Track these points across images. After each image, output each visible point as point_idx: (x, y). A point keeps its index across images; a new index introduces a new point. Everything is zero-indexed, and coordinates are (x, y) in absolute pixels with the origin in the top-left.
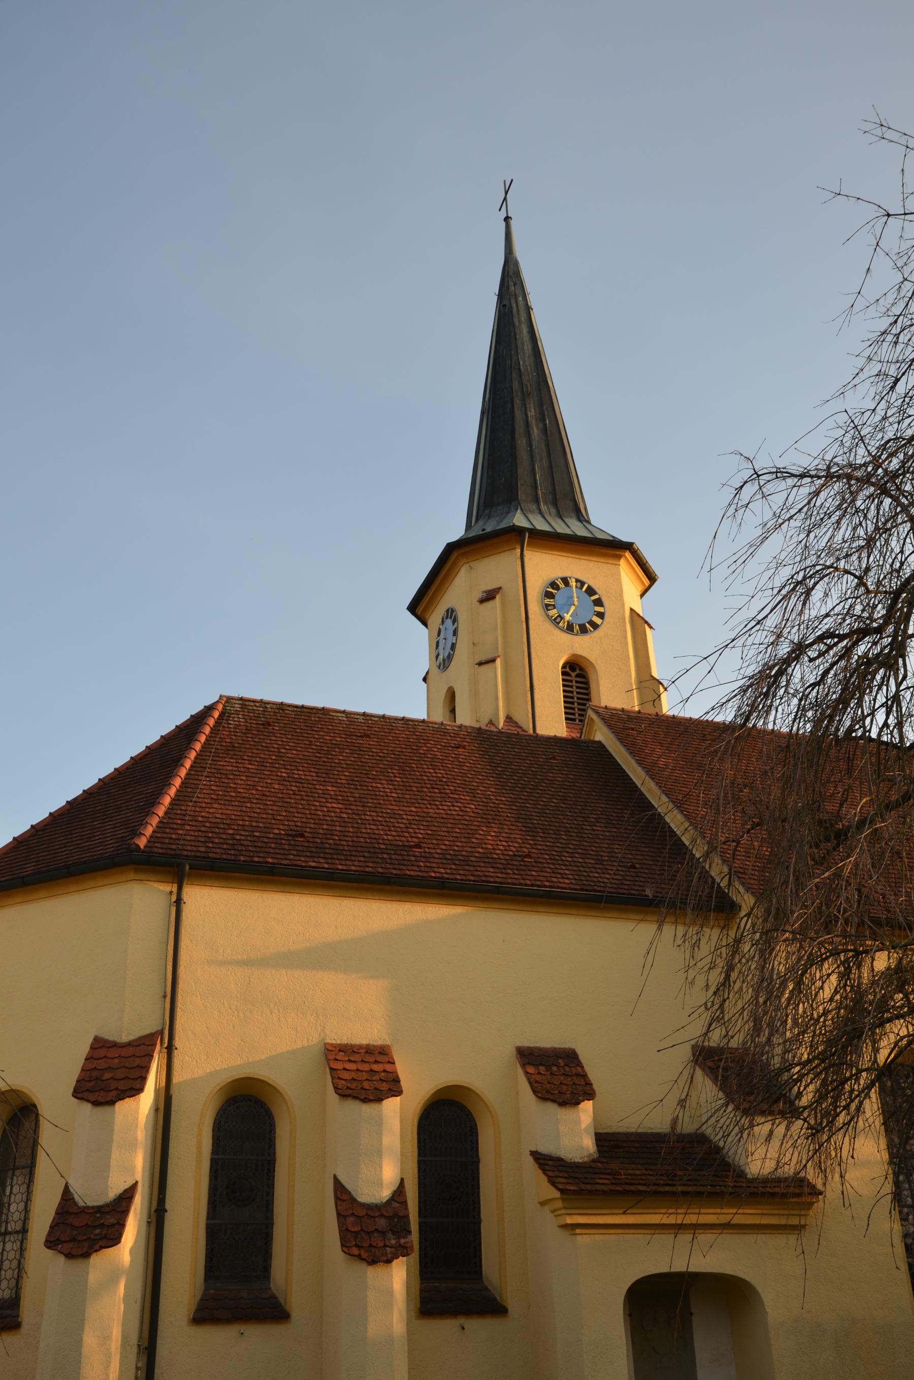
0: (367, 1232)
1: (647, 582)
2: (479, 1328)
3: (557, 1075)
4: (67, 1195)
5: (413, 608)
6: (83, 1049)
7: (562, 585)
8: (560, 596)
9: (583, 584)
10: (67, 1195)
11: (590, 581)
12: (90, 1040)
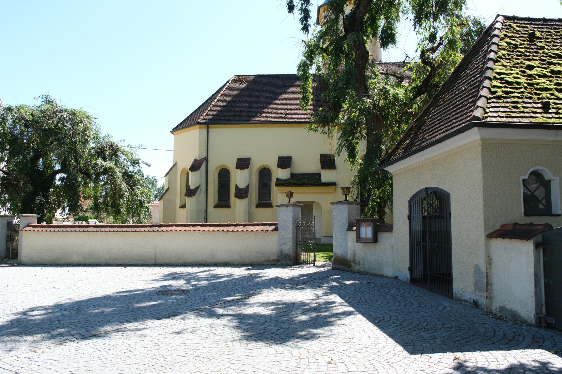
2: (268, 210)
4: (237, 187)
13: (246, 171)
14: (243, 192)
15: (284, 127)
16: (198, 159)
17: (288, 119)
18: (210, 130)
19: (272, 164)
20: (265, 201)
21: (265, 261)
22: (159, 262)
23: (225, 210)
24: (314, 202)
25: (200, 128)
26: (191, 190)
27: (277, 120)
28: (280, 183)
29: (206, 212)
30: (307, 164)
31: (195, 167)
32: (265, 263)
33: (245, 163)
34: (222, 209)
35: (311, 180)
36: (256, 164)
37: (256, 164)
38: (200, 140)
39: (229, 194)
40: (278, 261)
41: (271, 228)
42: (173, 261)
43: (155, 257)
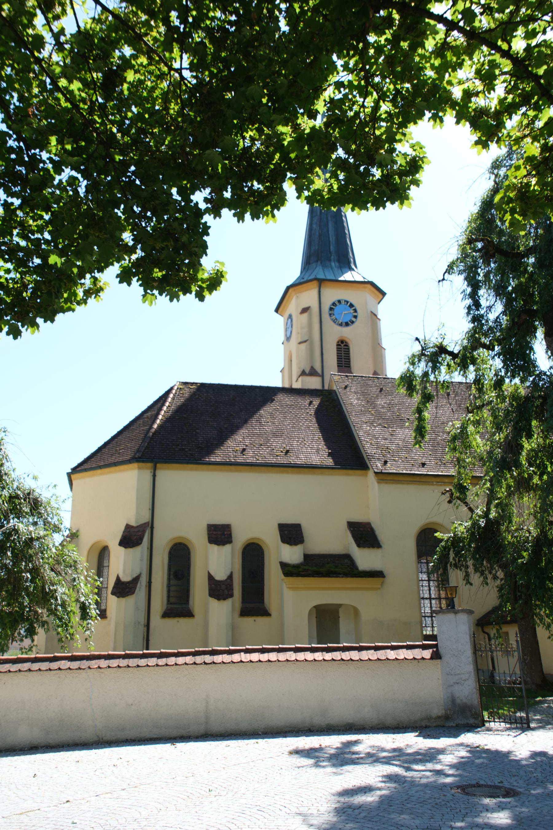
0: (219, 590)
1: (381, 296)
2: (261, 620)
3: (291, 534)
4: (118, 578)
5: (277, 310)
6: (122, 528)
7: (337, 304)
8: (337, 309)
9: (348, 302)
10: (118, 578)
11: (352, 300)
12: (125, 525)
13: (228, 547)
14: (223, 587)
15: (287, 472)
16: (133, 523)
17: (293, 460)
18: (158, 473)
19: (270, 539)
20: (254, 603)
21: (422, 720)
22: (215, 728)
23: (183, 622)
24: (340, 606)
25: (139, 468)
26: (123, 583)
27: (274, 461)
28: (289, 570)
29: (148, 625)
30: (328, 537)
31: (130, 538)
32: (424, 724)
33: (223, 534)
34: (176, 619)
35: (336, 566)
36: (241, 537)
37: (241, 537)
38: (139, 491)
39: (244, 588)
40: (447, 718)
41: (427, 654)
42: (244, 726)
43: (207, 718)
